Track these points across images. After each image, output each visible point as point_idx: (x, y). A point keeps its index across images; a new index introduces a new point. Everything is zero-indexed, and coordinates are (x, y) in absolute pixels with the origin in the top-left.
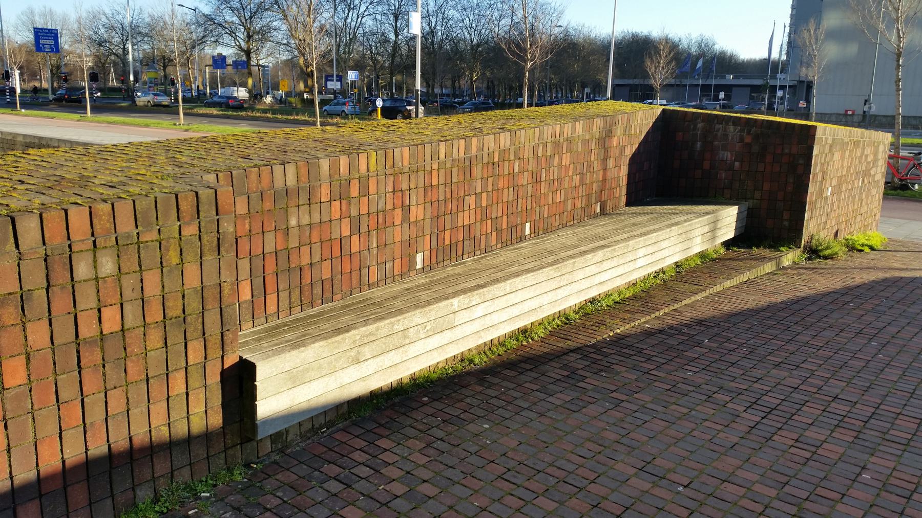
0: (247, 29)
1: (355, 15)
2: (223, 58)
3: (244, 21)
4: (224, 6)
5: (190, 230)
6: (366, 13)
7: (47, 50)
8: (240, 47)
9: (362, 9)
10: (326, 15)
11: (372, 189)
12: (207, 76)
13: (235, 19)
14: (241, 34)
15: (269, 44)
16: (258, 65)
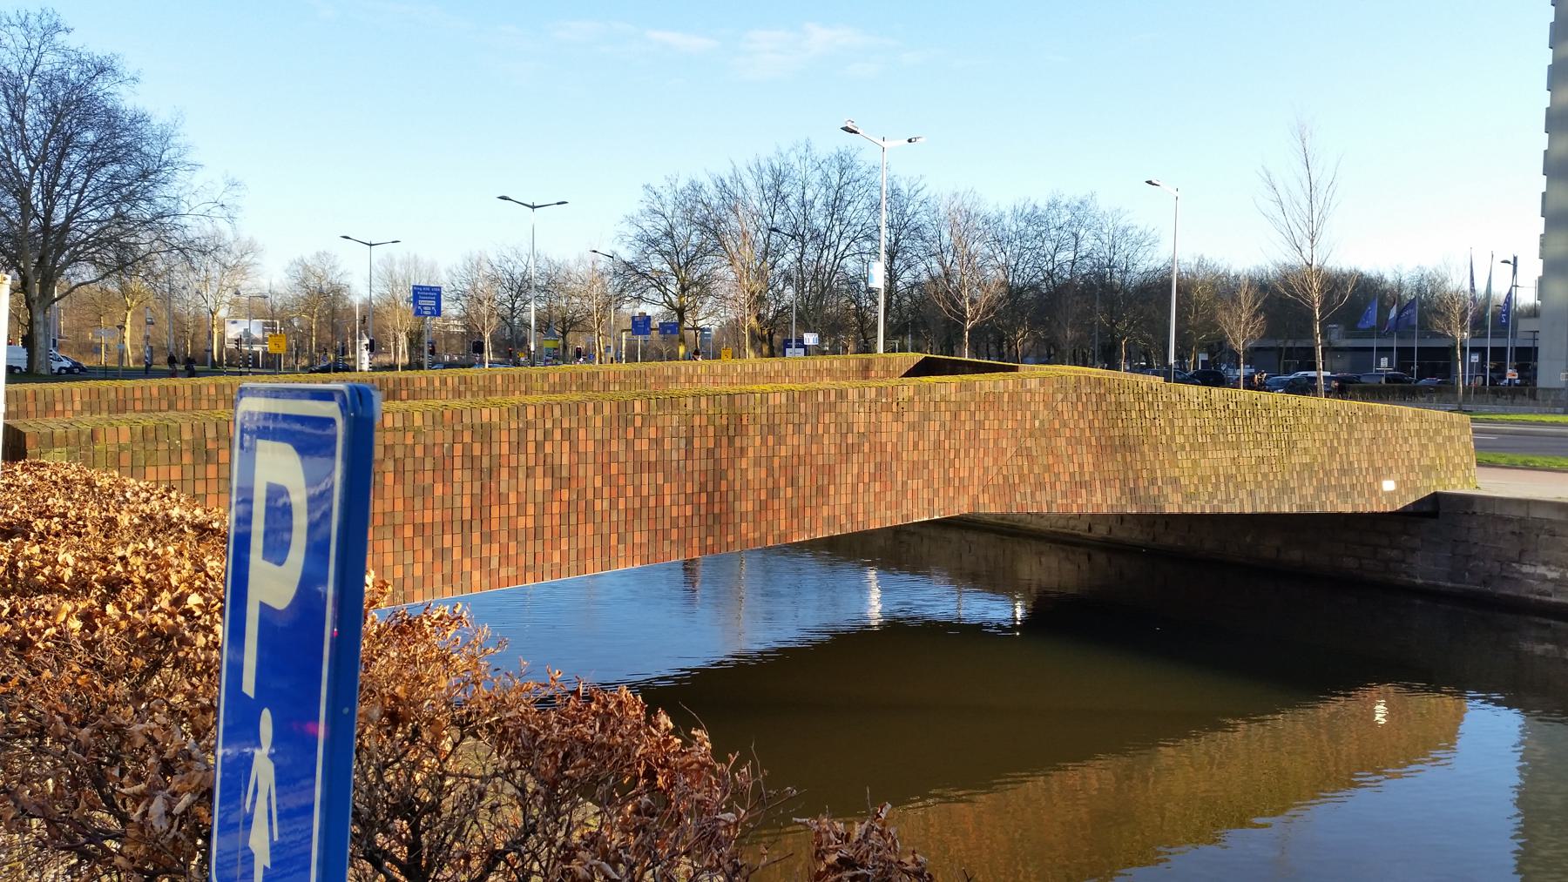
0: (681, 281)
1: (831, 257)
2: (647, 319)
3: (676, 267)
4: (651, 249)
5: (638, 381)
6: (847, 252)
7: (426, 313)
8: (671, 304)
9: (842, 248)
10: (790, 257)
11: (703, 380)
12: (624, 345)
13: (666, 267)
14: (673, 288)
15: (710, 300)
16: (695, 328)
